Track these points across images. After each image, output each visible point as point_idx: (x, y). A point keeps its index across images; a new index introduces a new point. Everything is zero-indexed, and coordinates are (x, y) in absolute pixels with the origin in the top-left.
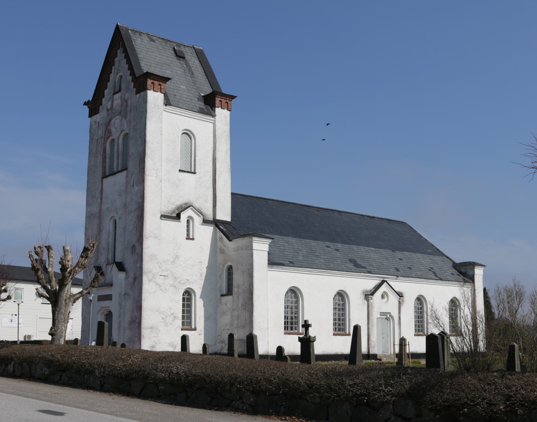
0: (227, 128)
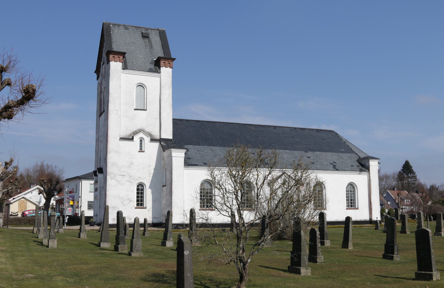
0: (170, 79)
